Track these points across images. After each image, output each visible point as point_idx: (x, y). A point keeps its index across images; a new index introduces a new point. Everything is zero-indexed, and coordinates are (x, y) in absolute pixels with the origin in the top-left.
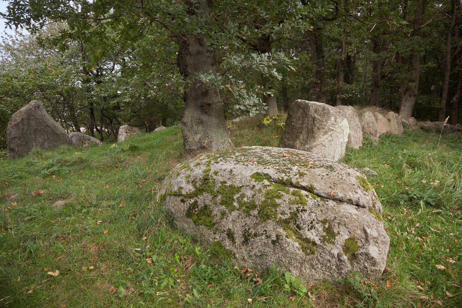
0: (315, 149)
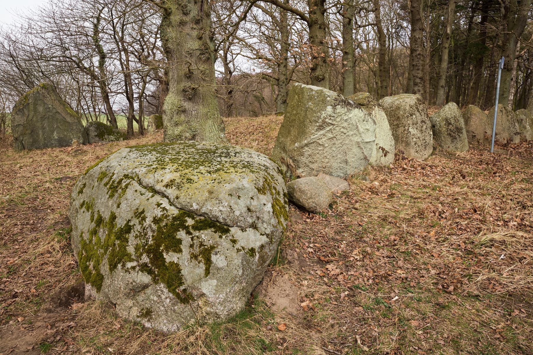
0: (306, 148)
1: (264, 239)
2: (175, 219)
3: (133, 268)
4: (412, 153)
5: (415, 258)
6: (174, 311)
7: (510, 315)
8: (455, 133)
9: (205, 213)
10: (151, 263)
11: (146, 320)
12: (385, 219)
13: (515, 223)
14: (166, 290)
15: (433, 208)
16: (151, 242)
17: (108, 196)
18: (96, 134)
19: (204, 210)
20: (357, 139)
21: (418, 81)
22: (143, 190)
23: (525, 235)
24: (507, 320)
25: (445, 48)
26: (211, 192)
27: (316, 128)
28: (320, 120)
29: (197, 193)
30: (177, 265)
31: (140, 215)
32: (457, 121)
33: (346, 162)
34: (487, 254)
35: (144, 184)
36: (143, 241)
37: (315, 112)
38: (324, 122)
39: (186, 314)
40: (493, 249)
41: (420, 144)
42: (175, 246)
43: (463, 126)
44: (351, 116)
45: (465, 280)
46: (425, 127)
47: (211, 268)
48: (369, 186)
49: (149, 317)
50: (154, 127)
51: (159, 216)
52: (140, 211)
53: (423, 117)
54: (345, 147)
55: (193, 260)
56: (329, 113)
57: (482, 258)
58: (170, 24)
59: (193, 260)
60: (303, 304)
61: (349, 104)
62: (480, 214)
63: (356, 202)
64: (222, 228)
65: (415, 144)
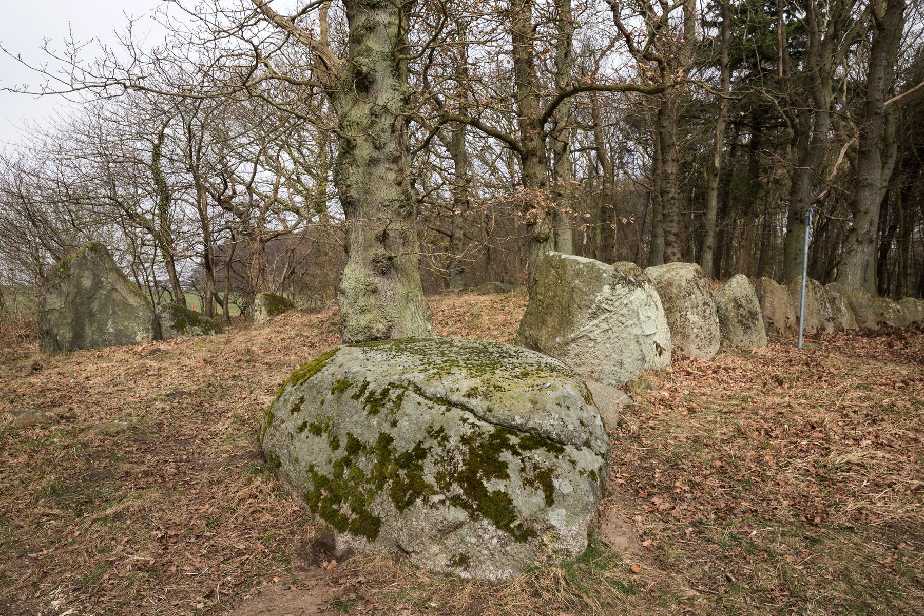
0: (573, 345)
1: (600, 461)
2: (492, 437)
3: (443, 502)
4: (693, 350)
5: (758, 487)
6: (505, 553)
7: (896, 548)
8: (747, 320)
9: (533, 428)
10: (466, 493)
11: (461, 569)
12: (696, 440)
13: (869, 442)
14: (492, 528)
15: (755, 426)
16: (461, 467)
17: (365, 413)
18: (173, 324)
19: (531, 424)
20: (636, 331)
21: (672, 238)
22: (430, 403)
23: (887, 456)
24: (894, 554)
25: (713, 189)
26: (534, 402)
27: (588, 316)
28: (594, 306)
29: (516, 403)
30: (506, 494)
31: (440, 434)
32: (749, 301)
33: (621, 364)
34: (845, 480)
35: (428, 394)
36: (449, 468)
37: (586, 293)
38: (599, 308)
39: (522, 556)
40: (851, 474)
41: (703, 337)
42: (501, 471)
43: (759, 309)
44: (632, 298)
45: (832, 510)
46: (708, 311)
47: (554, 495)
48: (658, 397)
49: (465, 565)
50: (264, 312)
51: (469, 434)
52: (437, 428)
53: (705, 297)
54: (621, 342)
55: (527, 487)
56: (606, 295)
57: (841, 485)
58: (354, 162)
59: (527, 487)
60: (645, 544)
61: (630, 282)
62: (821, 432)
63: (648, 419)
64: (555, 445)
65: (697, 336)
